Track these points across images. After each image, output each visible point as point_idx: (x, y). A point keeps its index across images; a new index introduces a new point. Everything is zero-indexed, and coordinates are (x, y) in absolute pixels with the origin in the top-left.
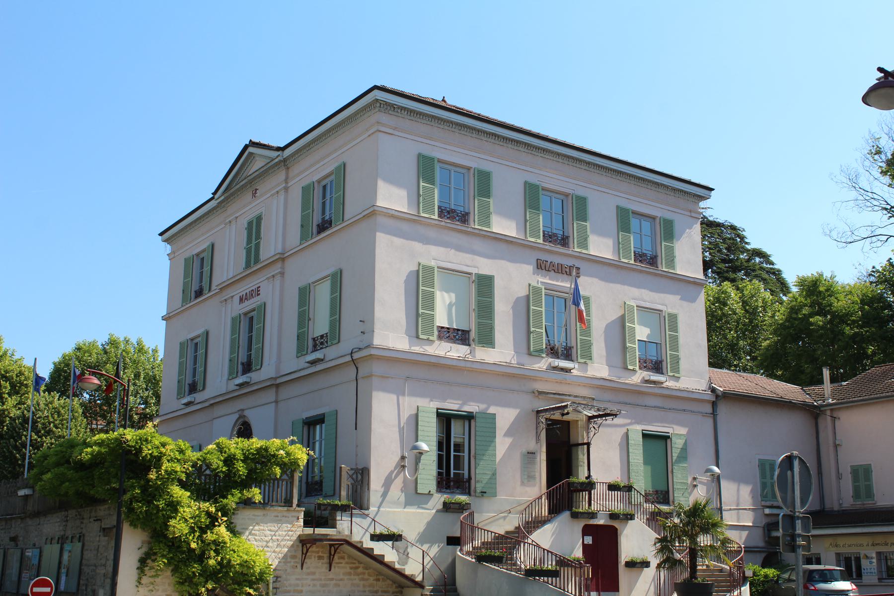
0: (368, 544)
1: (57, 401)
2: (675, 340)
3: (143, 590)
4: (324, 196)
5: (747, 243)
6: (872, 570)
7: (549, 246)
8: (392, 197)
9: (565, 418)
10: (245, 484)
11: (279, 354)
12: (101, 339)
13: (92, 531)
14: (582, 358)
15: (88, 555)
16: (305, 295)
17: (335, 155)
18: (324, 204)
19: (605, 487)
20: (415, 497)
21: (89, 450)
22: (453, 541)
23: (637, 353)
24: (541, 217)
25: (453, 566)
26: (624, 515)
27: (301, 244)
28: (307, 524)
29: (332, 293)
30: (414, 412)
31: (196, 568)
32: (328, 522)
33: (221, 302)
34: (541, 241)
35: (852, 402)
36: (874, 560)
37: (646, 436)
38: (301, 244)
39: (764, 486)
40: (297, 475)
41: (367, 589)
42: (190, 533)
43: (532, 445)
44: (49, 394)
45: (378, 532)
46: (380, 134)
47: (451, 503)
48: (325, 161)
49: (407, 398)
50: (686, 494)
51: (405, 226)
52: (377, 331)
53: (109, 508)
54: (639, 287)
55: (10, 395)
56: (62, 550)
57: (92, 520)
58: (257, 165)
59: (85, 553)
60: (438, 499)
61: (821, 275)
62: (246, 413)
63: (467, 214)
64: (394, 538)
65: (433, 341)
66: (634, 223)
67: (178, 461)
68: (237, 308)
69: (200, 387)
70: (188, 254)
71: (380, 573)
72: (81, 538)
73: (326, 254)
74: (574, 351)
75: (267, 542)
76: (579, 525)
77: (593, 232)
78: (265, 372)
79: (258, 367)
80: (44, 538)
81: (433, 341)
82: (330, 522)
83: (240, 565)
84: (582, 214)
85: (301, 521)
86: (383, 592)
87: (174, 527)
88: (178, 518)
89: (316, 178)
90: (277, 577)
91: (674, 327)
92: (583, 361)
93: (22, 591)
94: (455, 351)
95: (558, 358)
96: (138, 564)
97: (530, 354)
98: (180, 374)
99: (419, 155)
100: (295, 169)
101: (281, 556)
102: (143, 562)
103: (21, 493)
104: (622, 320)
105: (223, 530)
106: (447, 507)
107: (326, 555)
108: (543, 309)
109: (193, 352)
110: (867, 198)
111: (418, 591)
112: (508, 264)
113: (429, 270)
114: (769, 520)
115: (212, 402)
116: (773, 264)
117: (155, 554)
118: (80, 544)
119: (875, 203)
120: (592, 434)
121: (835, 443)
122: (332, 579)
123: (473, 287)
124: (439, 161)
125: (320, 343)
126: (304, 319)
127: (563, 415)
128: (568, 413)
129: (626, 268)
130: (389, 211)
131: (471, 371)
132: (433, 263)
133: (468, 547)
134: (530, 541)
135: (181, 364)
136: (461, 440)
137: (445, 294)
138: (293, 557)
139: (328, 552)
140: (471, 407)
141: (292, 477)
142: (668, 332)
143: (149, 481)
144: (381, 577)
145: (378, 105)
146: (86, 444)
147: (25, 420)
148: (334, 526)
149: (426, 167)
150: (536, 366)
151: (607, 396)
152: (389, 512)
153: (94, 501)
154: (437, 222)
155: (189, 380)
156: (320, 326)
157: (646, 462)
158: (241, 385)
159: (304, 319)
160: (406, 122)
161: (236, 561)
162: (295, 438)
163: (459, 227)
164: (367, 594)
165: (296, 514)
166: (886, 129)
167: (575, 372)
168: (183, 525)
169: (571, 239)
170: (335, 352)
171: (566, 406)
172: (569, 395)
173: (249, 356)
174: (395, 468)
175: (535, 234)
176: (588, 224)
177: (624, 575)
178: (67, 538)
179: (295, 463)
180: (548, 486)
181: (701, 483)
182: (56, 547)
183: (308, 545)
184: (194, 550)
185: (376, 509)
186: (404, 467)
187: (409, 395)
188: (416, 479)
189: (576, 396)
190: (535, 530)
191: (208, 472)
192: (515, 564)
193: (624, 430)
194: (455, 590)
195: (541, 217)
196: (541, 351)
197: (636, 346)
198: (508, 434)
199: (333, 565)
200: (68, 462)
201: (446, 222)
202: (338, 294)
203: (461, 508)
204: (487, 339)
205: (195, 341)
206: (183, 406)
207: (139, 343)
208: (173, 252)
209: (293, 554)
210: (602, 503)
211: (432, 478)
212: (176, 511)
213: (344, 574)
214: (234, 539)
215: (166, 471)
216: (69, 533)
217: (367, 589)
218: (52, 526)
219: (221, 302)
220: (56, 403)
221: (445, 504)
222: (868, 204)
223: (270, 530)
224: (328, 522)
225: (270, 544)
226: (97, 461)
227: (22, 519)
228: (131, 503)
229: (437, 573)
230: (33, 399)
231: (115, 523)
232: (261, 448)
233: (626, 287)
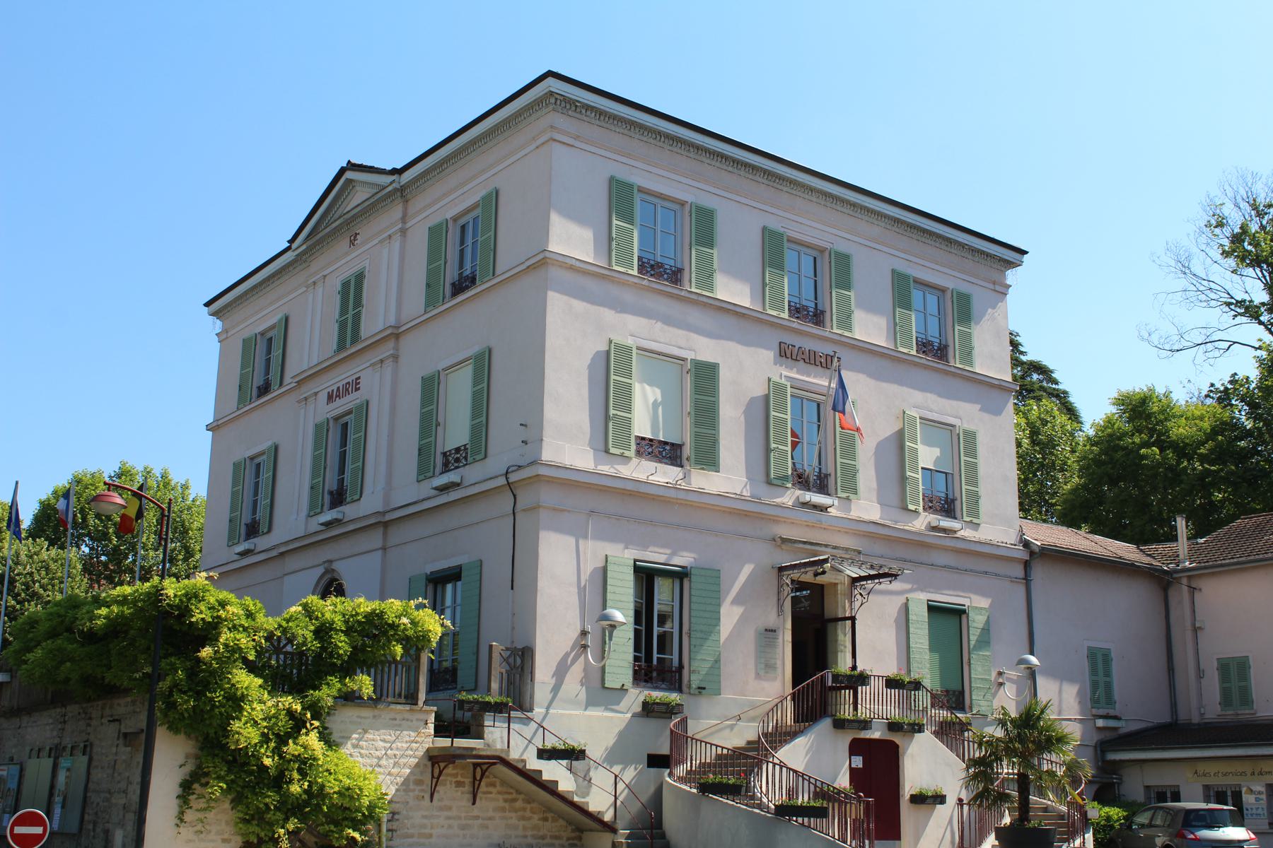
0: (533, 763)
1: (48, 553)
2: (973, 469)
3: (186, 832)
4: (462, 242)
5: (1022, 353)
6: (1260, 811)
7: (796, 324)
8: (571, 239)
10: (347, 670)
11: (389, 476)
12: (108, 469)
13: (106, 738)
15: (97, 775)
16: (431, 387)
18: (462, 252)
19: (882, 683)
20: (601, 692)
21: (104, 611)
22: (657, 761)
23: (921, 487)
24: (786, 280)
25: (657, 799)
26: (909, 724)
27: (426, 312)
28: (440, 731)
30: (602, 564)
31: (272, 798)
32: (472, 729)
33: (299, 402)
35: (1222, 565)
37: (933, 609)
38: (426, 312)
39: (1095, 686)
40: (425, 656)
41: (530, 833)
42: (261, 743)
43: (771, 619)
44: (34, 540)
45: (549, 745)
46: (555, 145)
47: (655, 703)
48: (466, 189)
49: (590, 543)
50: (989, 696)
51: (590, 284)
53: (134, 702)
54: (923, 389)
56: (55, 767)
57: (105, 721)
58: (359, 196)
60: (636, 697)
62: (335, 566)
63: (680, 270)
65: (629, 458)
66: (916, 295)
67: (245, 629)
68: (323, 410)
69: (263, 527)
70: (247, 333)
71: (549, 809)
72: (87, 749)
73: (468, 326)
74: (831, 481)
75: (379, 759)
76: (845, 739)
77: (859, 306)
78: (368, 504)
80: (28, 749)
81: (629, 458)
82: (473, 729)
83: (339, 793)
84: (844, 280)
85: (431, 726)
87: (238, 733)
88: (244, 719)
89: (449, 215)
90: (394, 813)
91: (972, 452)
92: (844, 495)
94: (662, 475)
95: (809, 490)
96: (179, 791)
97: (769, 482)
100: (417, 203)
104: (900, 437)
105: (312, 740)
106: (649, 709)
107: (468, 781)
108: (789, 417)
109: (250, 482)
110: (1202, 288)
111: (607, 838)
112: (739, 347)
113: (625, 351)
114: (1102, 736)
115: (283, 549)
116: (1057, 383)
117: (207, 774)
118: (85, 759)
119: (1213, 296)
120: (857, 604)
121: (1194, 625)
122: (477, 817)
123: (688, 380)
124: (641, 190)
125: (455, 459)
126: (429, 423)
127: (816, 574)
128: (824, 572)
129: (904, 361)
130: (568, 261)
132: (630, 342)
133: (681, 770)
134: (776, 761)
135: (234, 494)
136: (669, 609)
138: (419, 782)
139: (471, 775)
140: (682, 559)
141: (418, 659)
142: (963, 458)
143: (199, 660)
144: (550, 815)
145: (553, 100)
149: (621, 198)
151: (879, 548)
152: (562, 715)
153: (112, 691)
154: (636, 280)
155: (247, 518)
156: (456, 433)
158: (328, 525)
159: (429, 423)
160: (593, 130)
161: (332, 787)
162: (425, 602)
163: (669, 289)
164: (530, 840)
165: (423, 716)
166: (1230, 194)
168: (250, 729)
169: (828, 315)
170: (479, 474)
171: (826, 561)
172: (826, 546)
173: (341, 481)
174: (572, 649)
176: (852, 294)
178: (64, 748)
179: (424, 638)
180: (795, 684)
181: (1009, 680)
182: (47, 763)
183: (442, 765)
185: (543, 710)
186: (585, 647)
189: (835, 548)
191: (289, 648)
192: (753, 797)
193: (902, 599)
194: (663, 836)
195: (786, 280)
196: (785, 478)
197: (920, 476)
199: (479, 795)
200: (70, 630)
201: (647, 281)
202: (485, 385)
203: (668, 711)
204: (708, 458)
205: (257, 461)
206: (237, 557)
210: (876, 706)
211: (626, 664)
212: (241, 709)
213: (495, 810)
214: (329, 753)
215: (226, 646)
216: (67, 741)
218: (40, 729)
219: (299, 402)
220: (44, 555)
221: (645, 705)
222: (1203, 297)
223: (384, 741)
225: (383, 762)
226: (116, 628)
228: (171, 694)
229: (636, 807)
230: (10, 549)
231: (144, 725)
233: (905, 389)
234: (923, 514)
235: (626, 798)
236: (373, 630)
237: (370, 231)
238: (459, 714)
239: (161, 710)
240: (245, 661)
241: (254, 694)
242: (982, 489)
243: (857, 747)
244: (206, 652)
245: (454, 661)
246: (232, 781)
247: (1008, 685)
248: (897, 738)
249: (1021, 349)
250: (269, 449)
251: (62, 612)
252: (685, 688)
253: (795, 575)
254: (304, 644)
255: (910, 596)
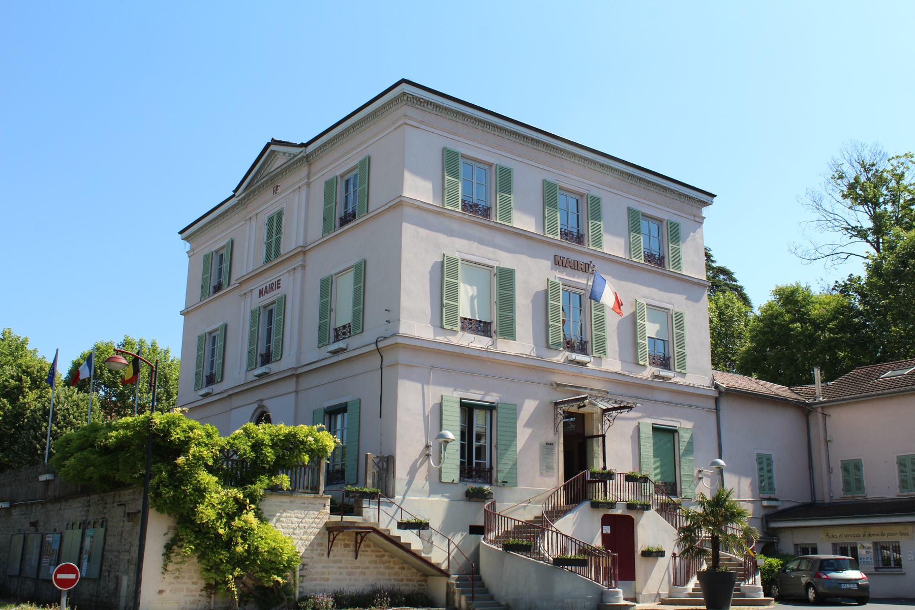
0: (395, 532)
2: (681, 337)
4: (347, 191)
5: (713, 261)
7: (565, 243)
8: (418, 189)
9: (582, 410)
10: (273, 471)
11: (300, 344)
13: (116, 515)
14: (597, 352)
15: (111, 540)
16: (326, 286)
17: (358, 150)
18: (346, 197)
19: (622, 478)
21: (114, 433)
22: (476, 530)
26: (641, 505)
28: (333, 511)
29: (356, 283)
30: (439, 401)
31: (224, 555)
32: (354, 510)
34: (558, 238)
35: (844, 400)
36: (871, 550)
37: (656, 430)
39: (761, 479)
40: (324, 462)
41: (392, 577)
42: (217, 519)
43: (550, 437)
45: (405, 520)
48: (349, 156)
49: (431, 388)
50: (692, 486)
52: (403, 320)
53: (134, 492)
54: (649, 286)
55: (30, 389)
57: (115, 505)
58: (279, 162)
59: (108, 538)
61: (798, 286)
62: (265, 403)
63: (489, 209)
64: (420, 526)
65: (456, 332)
66: (644, 224)
67: (206, 445)
68: (257, 302)
69: (218, 379)
70: (207, 251)
71: (405, 562)
72: (104, 523)
73: (351, 245)
74: (589, 345)
76: (598, 515)
77: (607, 231)
78: (286, 362)
79: (278, 358)
80: (65, 524)
81: (456, 332)
82: (355, 509)
84: (596, 214)
85: (328, 508)
86: (407, 580)
88: (206, 504)
89: (338, 173)
90: (304, 565)
91: (681, 326)
92: (597, 355)
93: (43, 575)
94: (478, 342)
96: (164, 551)
97: (548, 347)
98: (198, 366)
99: (444, 149)
100: (317, 165)
101: (308, 543)
102: (169, 548)
103: (42, 478)
105: (250, 517)
107: (352, 543)
109: (209, 348)
112: (528, 259)
113: (453, 262)
115: (230, 393)
117: (182, 540)
118: (103, 530)
119: (837, 224)
120: (606, 427)
122: (358, 567)
123: (495, 280)
124: (463, 156)
125: (342, 333)
126: (326, 309)
127: (579, 407)
128: (584, 406)
130: (416, 203)
131: (494, 362)
132: (457, 255)
133: (491, 536)
135: (198, 357)
136: (483, 430)
137: (468, 287)
138: (320, 545)
139: (354, 539)
140: (492, 398)
141: (319, 464)
142: (675, 330)
143: (176, 465)
144: (406, 566)
145: (405, 98)
146: (110, 427)
147: (46, 412)
148: (360, 514)
149: (451, 162)
150: (554, 359)
151: (620, 390)
153: (119, 486)
154: (460, 215)
155: (207, 372)
156: (343, 315)
157: (655, 455)
158: (260, 376)
159: (326, 309)
161: (264, 547)
163: (482, 221)
167: (590, 366)
169: (586, 237)
170: (358, 342)
171: (585, 398)
173: (268, 348)
175: (553, 231)
176: (601, 223)
177: (639, 561)
178: (89, 523)
179: (323, 450)
181: (706, 475)
182: (78, 533)
183: (335, 533)
184: (221, 535)
185: (401, 497)
186: (428, 455)
187: (435, 384)
188: (440, 470)
189: (592, 390)
190: (557, 520)
191: (235, 457)
192: (539, 553)
193: (635, 423)
196: (559, 344)
197: (647, 342)
198: (527, 425)
199: (360, 553)
200: (92, 445)
201: (468, 216)
204: (508, 331)
206: (201, 398)
207: (153, 345)
208: (192, 250)
209: (320, 541)
210: (619, 493)
212: (204, 497)
213: (370, 562)
215: (194, 456)
216: (91, 518)
217: (392, 577)
218: (74, 511)
220: (75, 397)
222: (831, 225)
223: (297, 517)
224: (354, 510)
225: (297, 531)
226: (122, 445)
227: (43, 504)
228: (158, 488)
229: (462, 560)
231: (141, 508)
232: (290, 432)
233: (636, 285)
234: (649, 367)
235: (456, 554)
236: (289, 446)
237: (283, 184)
238: (346, 500)
239: (152, 498)
240: (206, 465)
241: (212, 487)
242: (688, 351)
243: (606, 520)
244: (181, 460)
245: (342, 465)
246: (199, 544)
247: (705, 479)
248: (632, 514)
249: (712, 259)
250: (222, 326)
251: (87, 434)
252: (494, 482)
253: (566, 407)
254: (245, 454)
255: (640, 421)
